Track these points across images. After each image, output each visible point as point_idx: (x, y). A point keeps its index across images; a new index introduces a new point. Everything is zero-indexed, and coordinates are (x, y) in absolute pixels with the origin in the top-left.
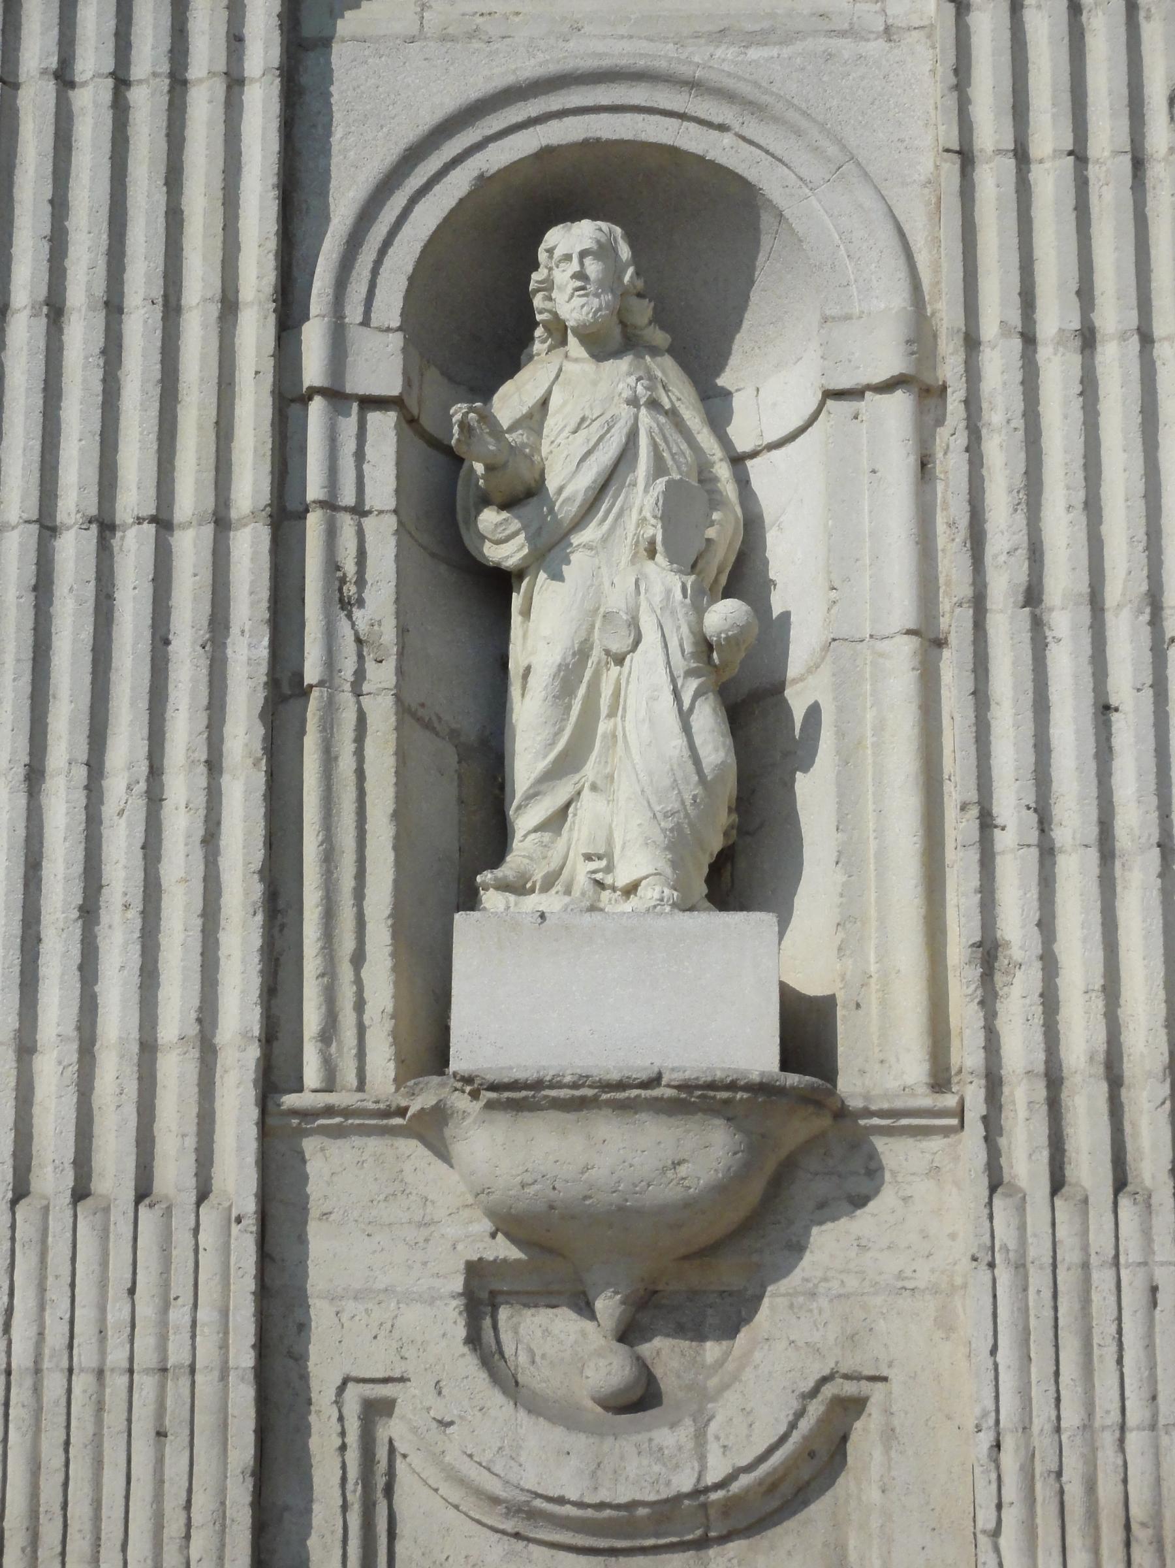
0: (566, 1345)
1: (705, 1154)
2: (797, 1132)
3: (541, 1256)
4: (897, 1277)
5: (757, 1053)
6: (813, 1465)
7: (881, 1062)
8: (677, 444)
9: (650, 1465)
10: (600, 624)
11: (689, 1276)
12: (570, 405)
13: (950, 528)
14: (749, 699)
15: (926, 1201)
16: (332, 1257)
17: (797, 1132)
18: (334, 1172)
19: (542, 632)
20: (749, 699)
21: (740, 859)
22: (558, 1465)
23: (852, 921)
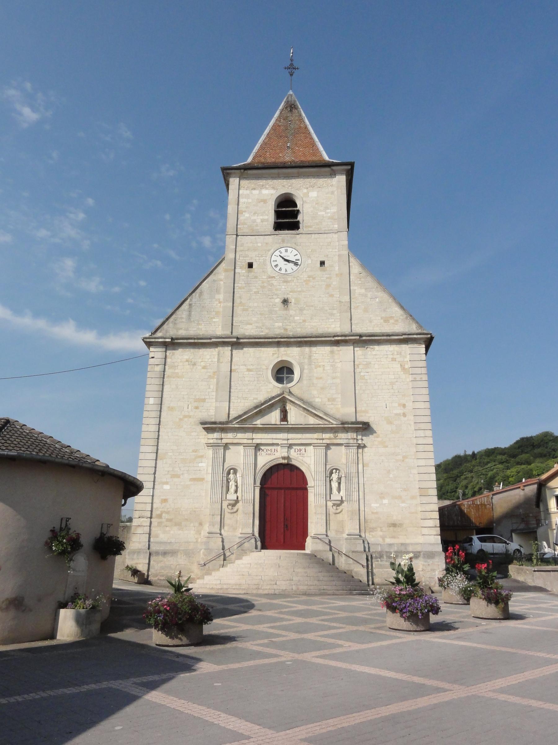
0: (230, 507)
1: (234, 502)
2: (237, 501)
3: (229, 505)
4: (239, 505)
5: (236, 499)
6: (237, 511)
7: (344, 499)
8: (512, 472)
9: (232, 511)
10: (232, 484)
11: (233, 505)
12: (231, 476)
13: (242, 482)
14: (237, 486)
15: (345, 504)
16: (223, 504)
17: (237, 501)
18: (328, 502)
19: (230, 484)
20: (237, 486)
21: (236, 492)
22: (229, 511)
23: (343, 493)
